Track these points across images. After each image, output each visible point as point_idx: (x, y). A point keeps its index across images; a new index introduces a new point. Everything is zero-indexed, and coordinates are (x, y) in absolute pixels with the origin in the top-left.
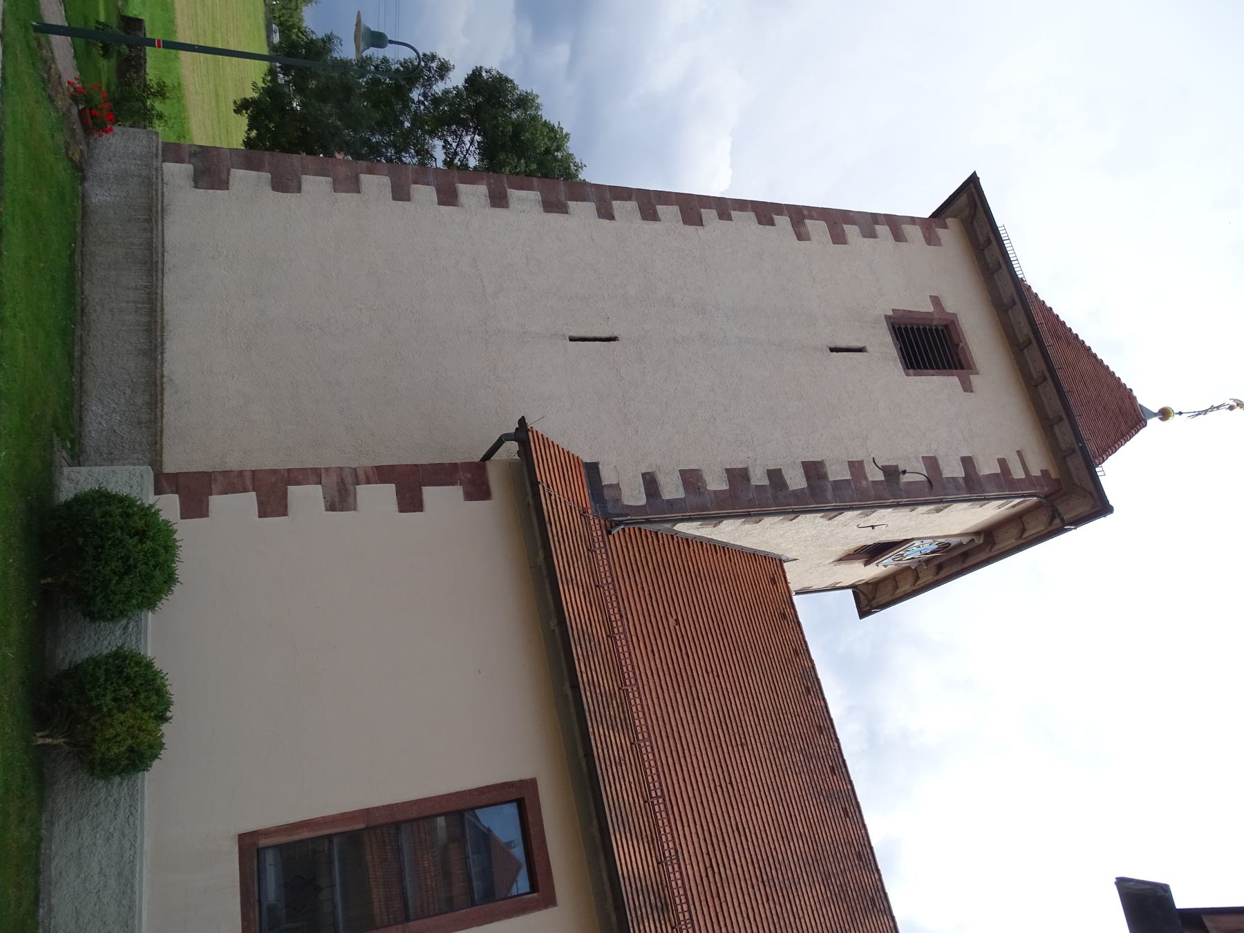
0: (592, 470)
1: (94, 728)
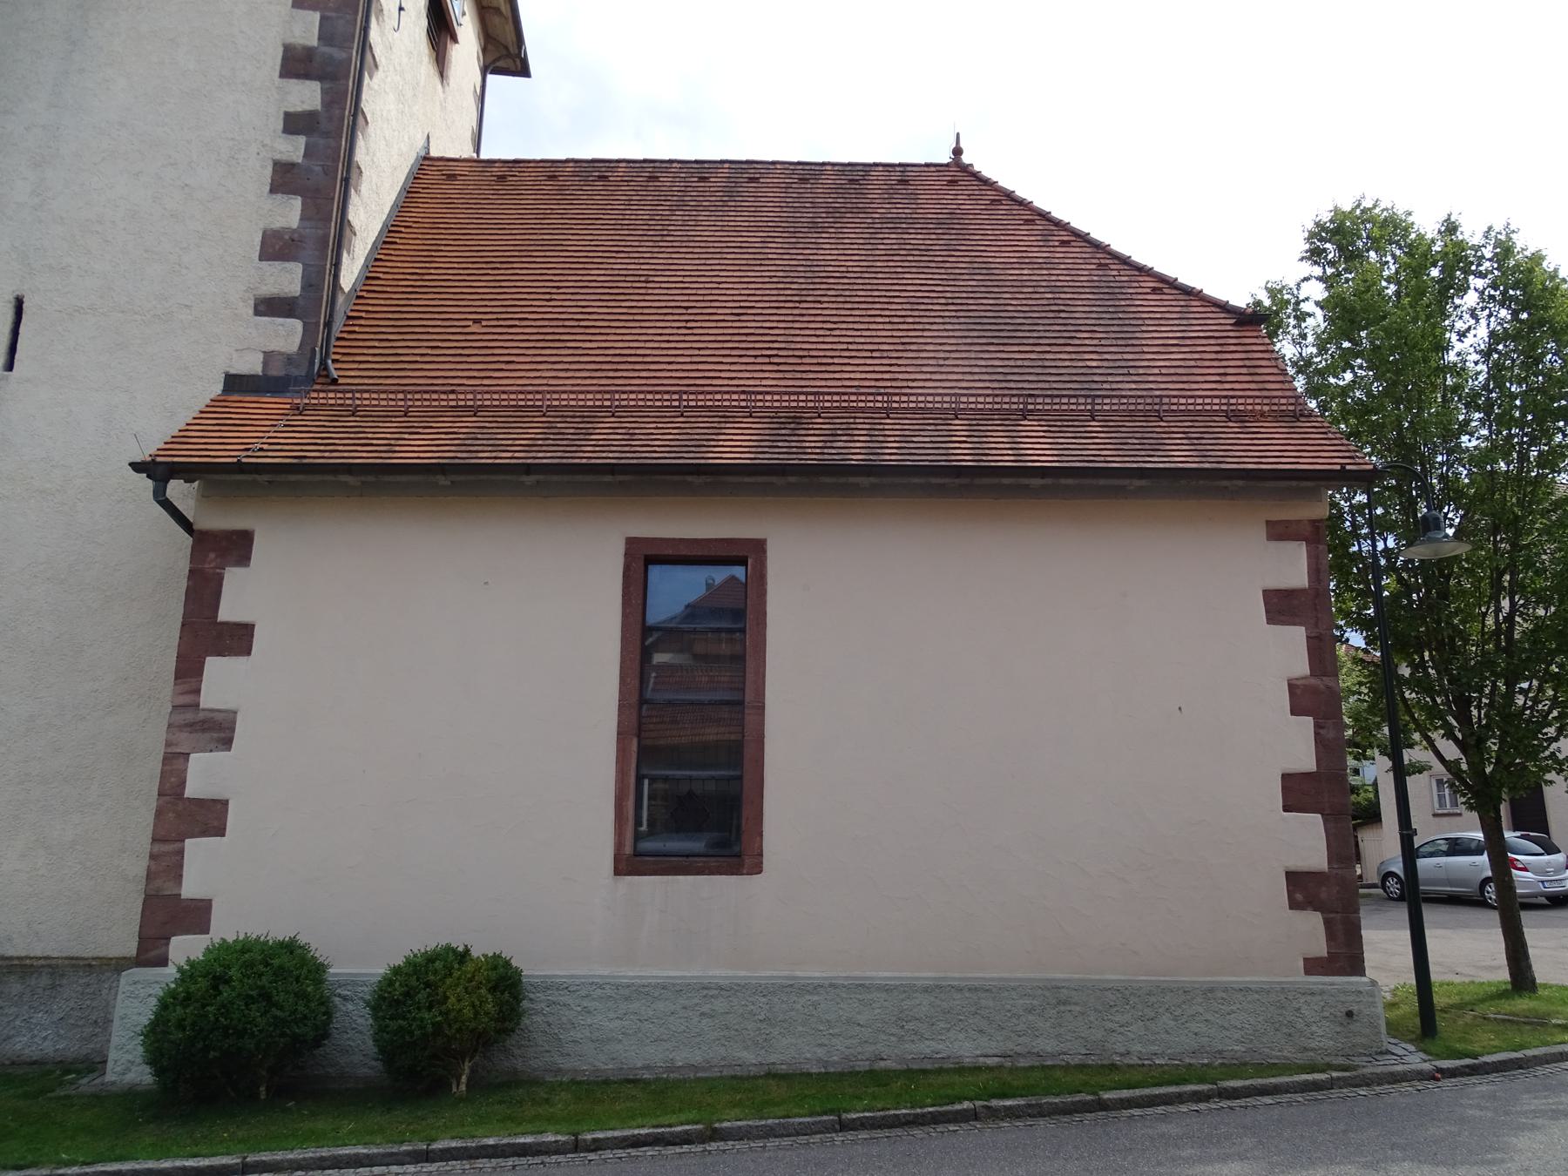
0: (235, 383)
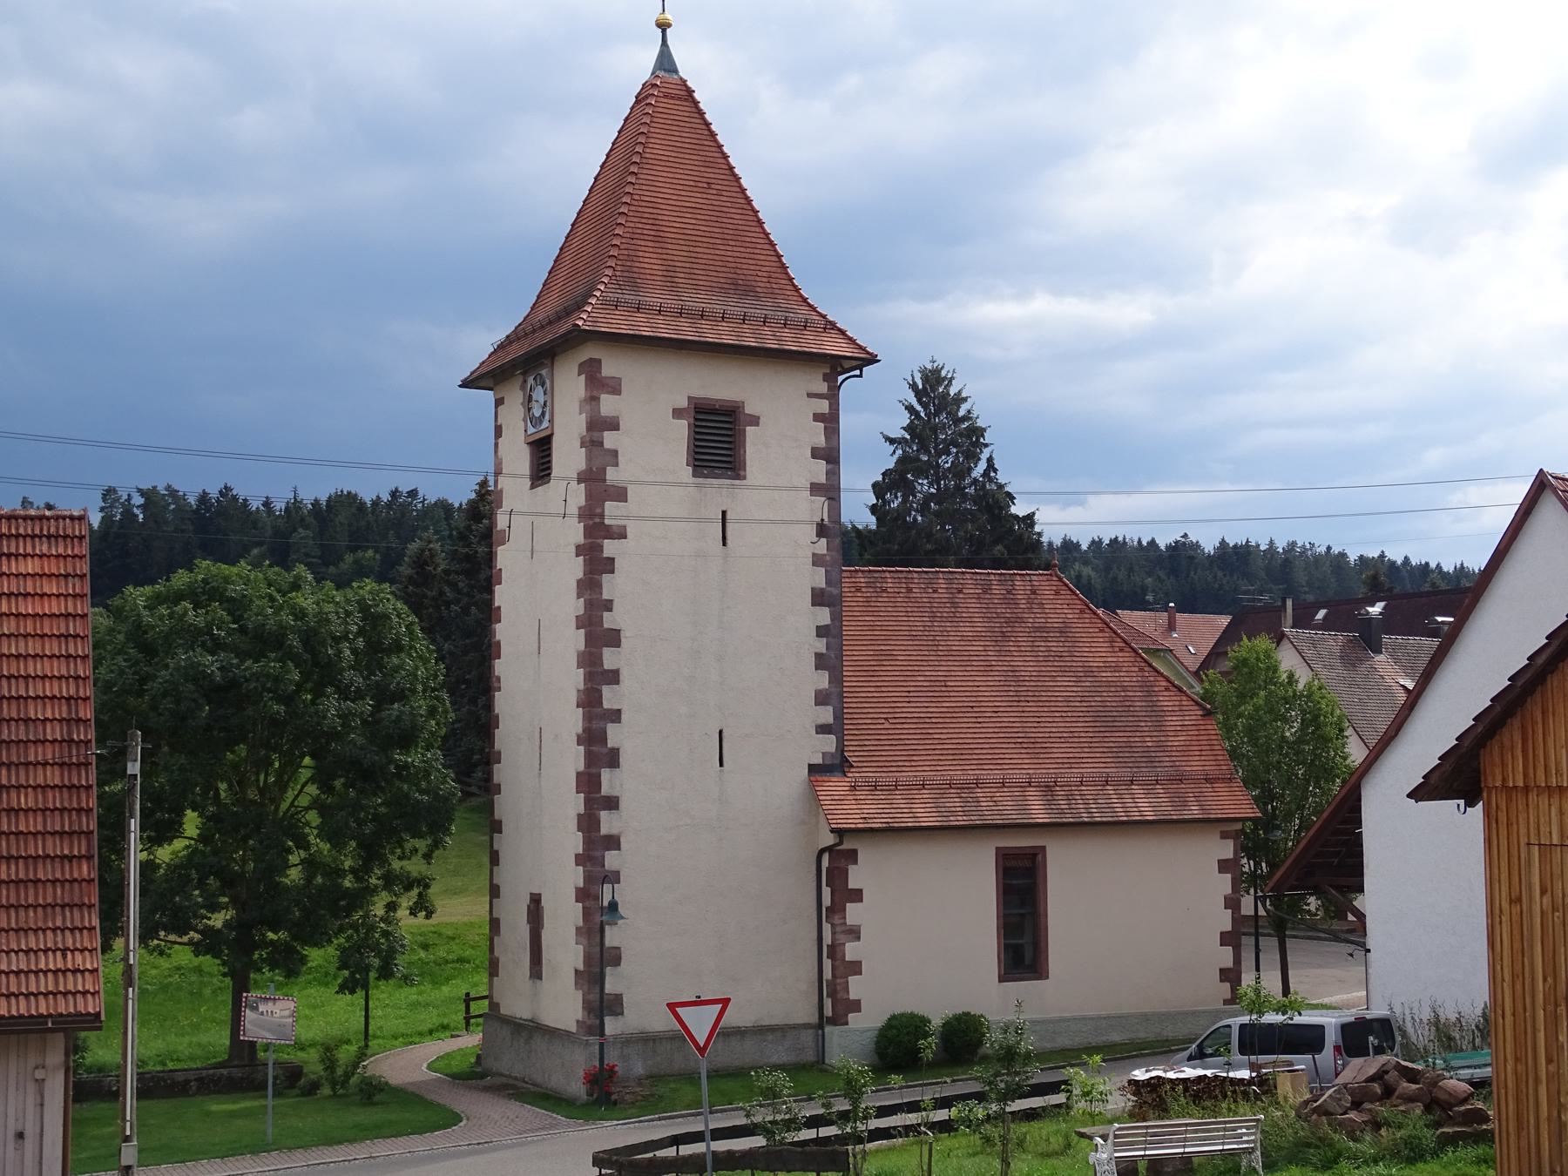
0: (813, 769)
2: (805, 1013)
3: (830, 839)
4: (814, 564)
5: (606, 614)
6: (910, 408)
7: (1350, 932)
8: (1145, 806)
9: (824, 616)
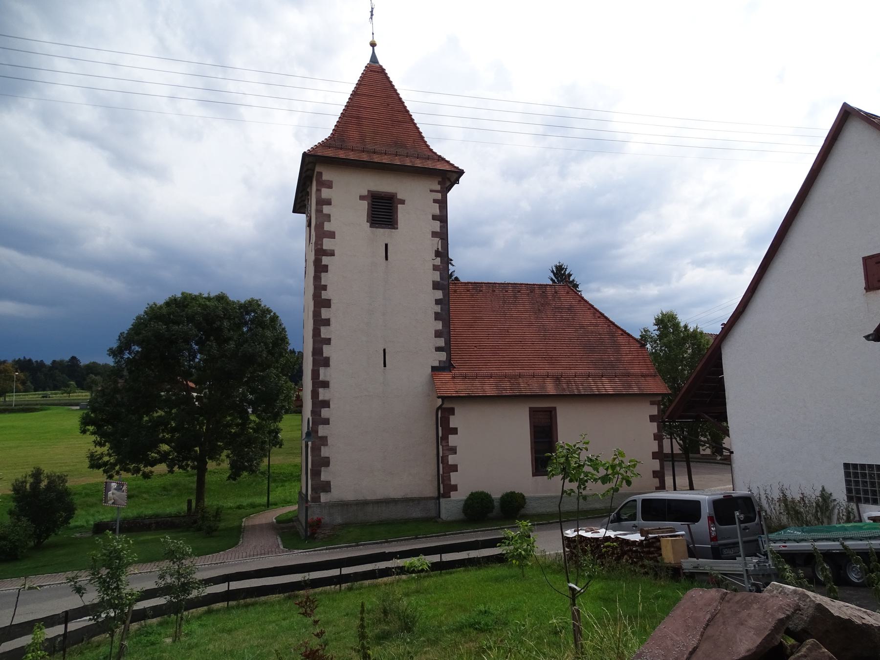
0: (434, 369)
1: (297, 624)
2: (430, 491)
3: (440, 402)
4: (434, 270)
5: (323, 292)
6: (552, 279)
7: (722, 458)
8: (608, 387)
9: (439, 294)
